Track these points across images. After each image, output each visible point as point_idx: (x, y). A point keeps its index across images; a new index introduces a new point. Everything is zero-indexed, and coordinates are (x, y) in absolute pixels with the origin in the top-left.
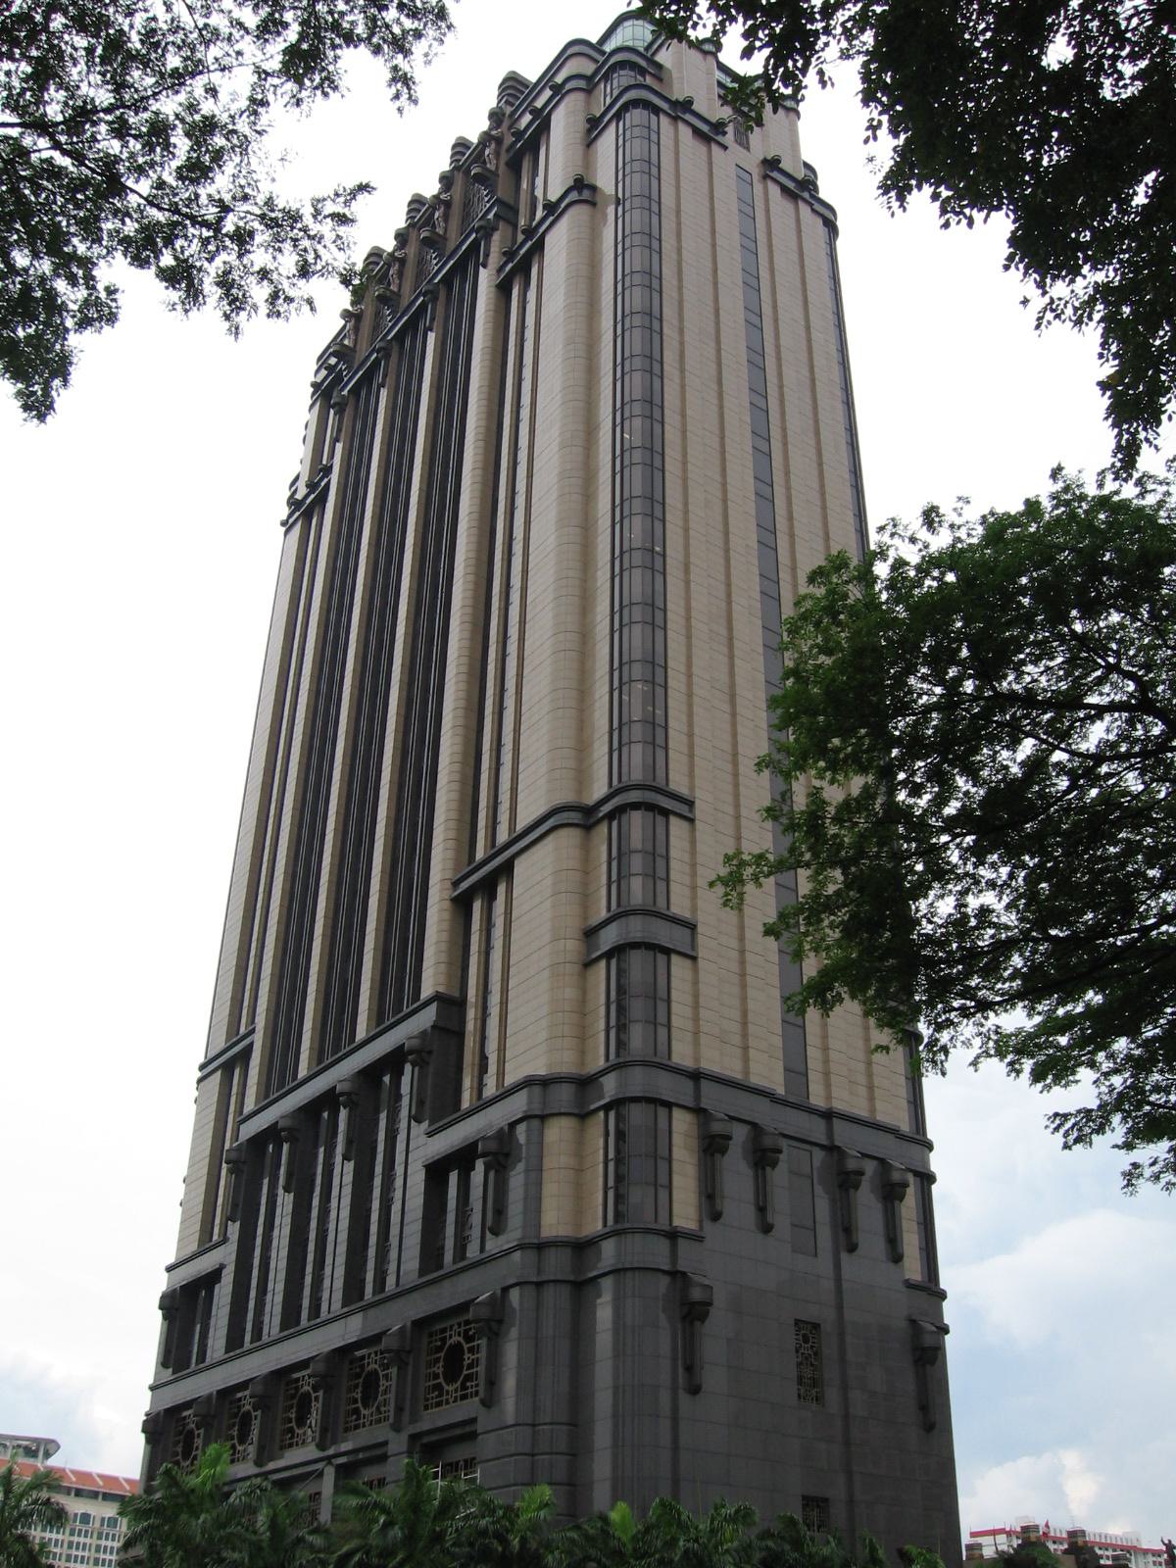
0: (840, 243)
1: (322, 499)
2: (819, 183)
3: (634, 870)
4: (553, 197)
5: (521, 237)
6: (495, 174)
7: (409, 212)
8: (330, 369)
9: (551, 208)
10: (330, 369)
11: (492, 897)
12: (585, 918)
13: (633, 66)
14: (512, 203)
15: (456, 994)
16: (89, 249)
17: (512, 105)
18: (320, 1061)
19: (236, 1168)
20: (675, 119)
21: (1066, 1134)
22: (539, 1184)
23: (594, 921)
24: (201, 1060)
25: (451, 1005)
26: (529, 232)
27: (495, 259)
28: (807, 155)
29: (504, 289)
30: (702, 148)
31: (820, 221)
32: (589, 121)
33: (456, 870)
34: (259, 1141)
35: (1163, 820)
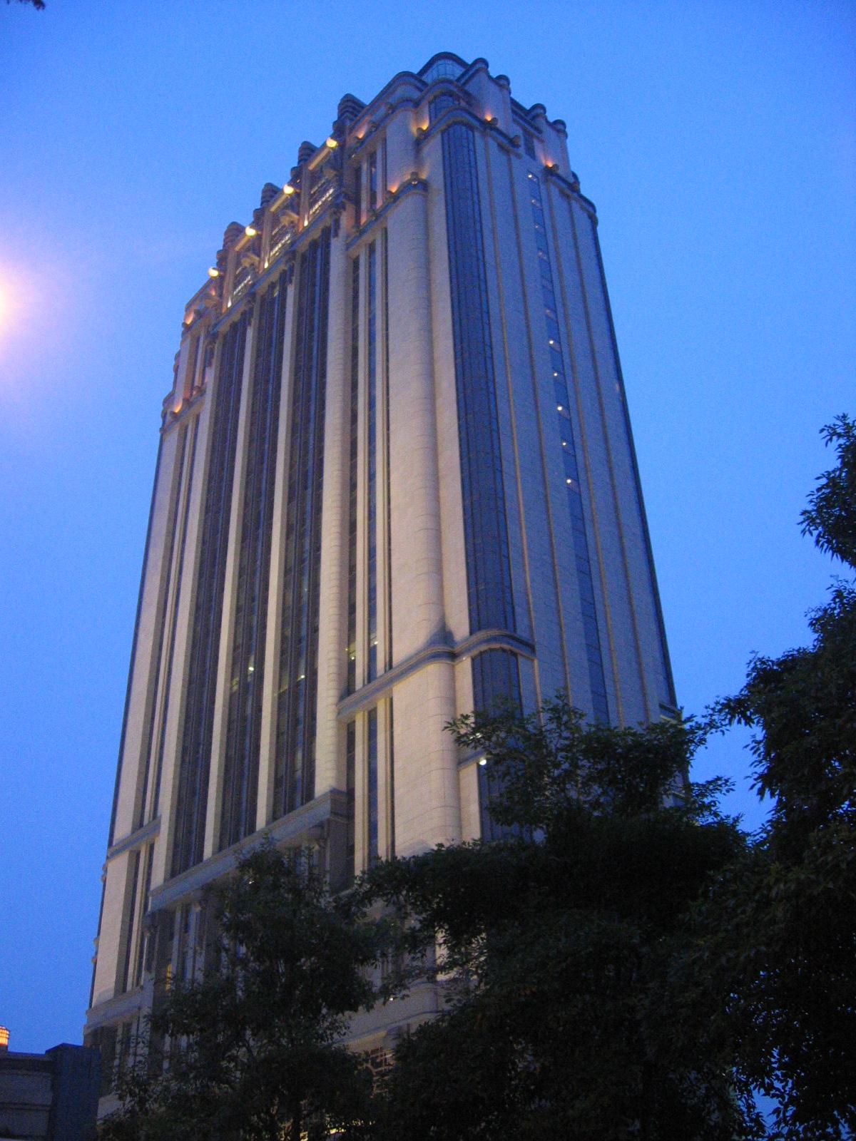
0: (599, 229)
7: (263, 198)
8: (364, 986)
10: (364, 986)
13: (451, 94)
16: (199, 969)
20: (484, 136)
21: (759, 755)
22: (352, 376)
25: (343, 799)
28: (574, 168)
30: (504, 158)
31: (585, 215)
35: (765, 687)
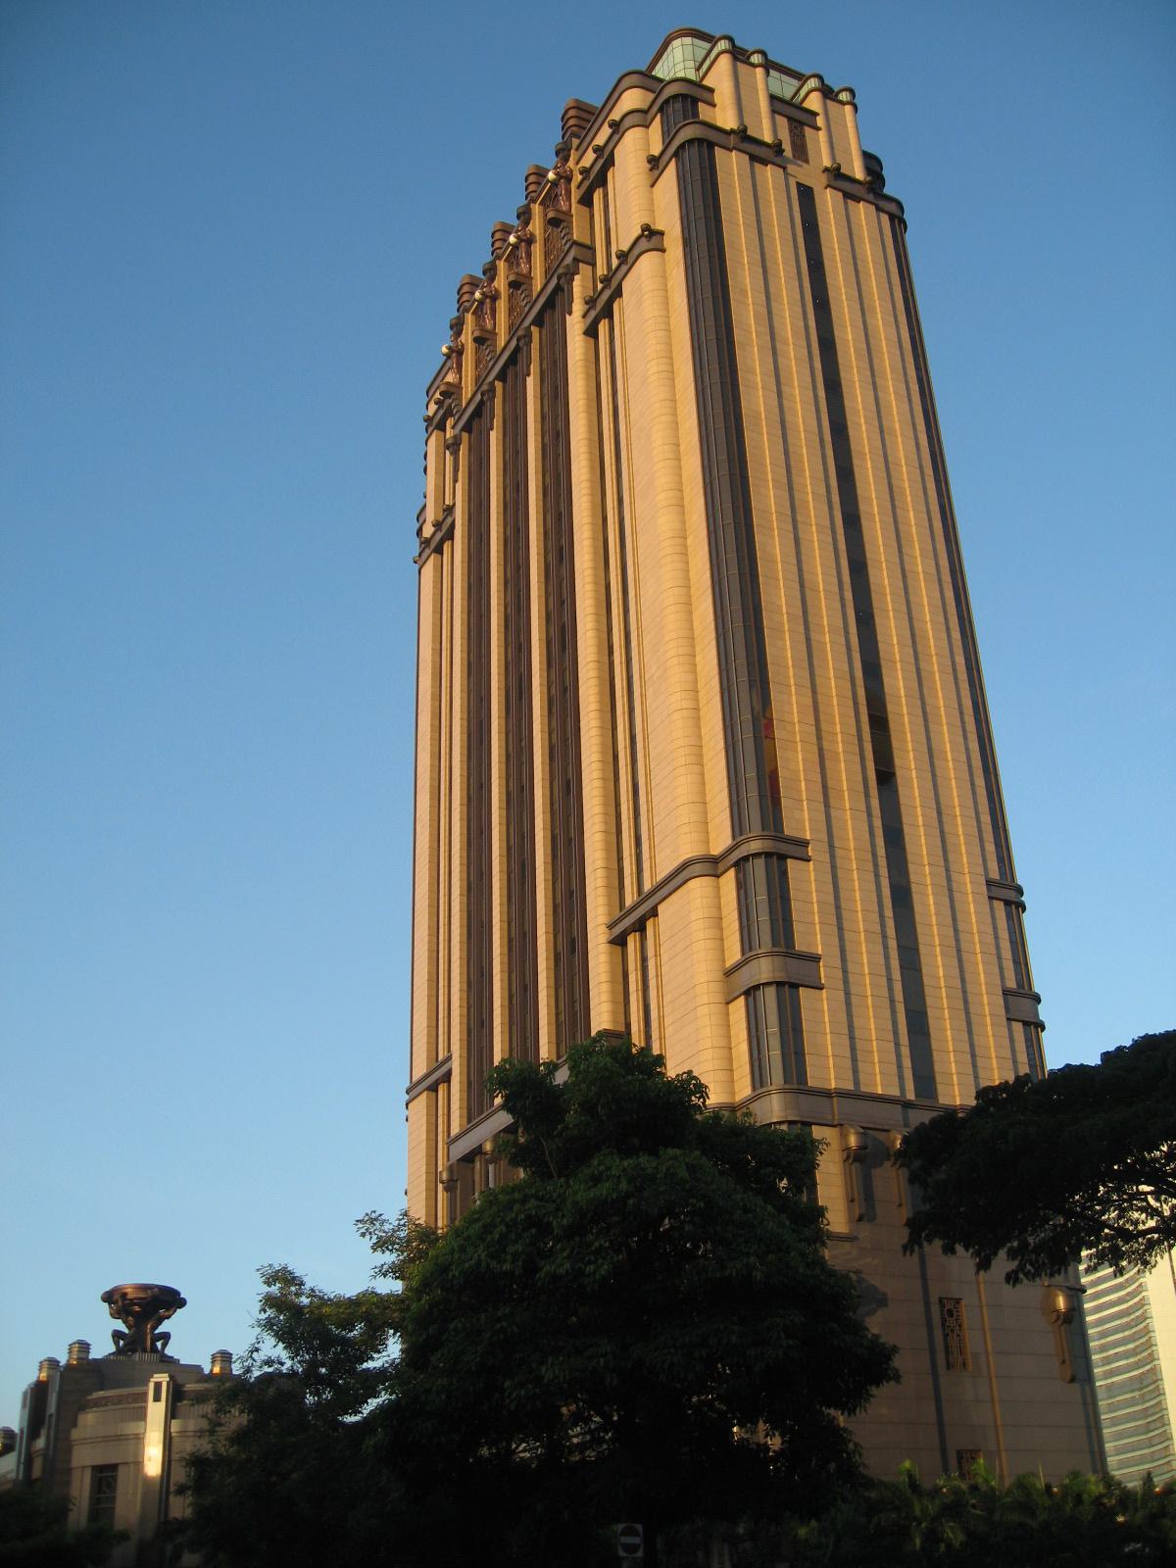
0: (910, 237)
1: (450, 535)
2: (884, 173)
3: (606, 1014)
4: (625, 247)
5: (600, 286)
6: (569, 214)
9: (623, 256)
11: (611, 317)
12: (724, 961)
14: (588, 242)
15: (622, 1028)
17: (578, 137)
18: (469, 1121)
19: (450, 1188)
23: (729, 964)
24: (407, 1084)
26: (606, 280)
27: (578, 307)
29: (591, 332)
32: (649, 162)
33: (610, 914)
34: (469, 1158)
